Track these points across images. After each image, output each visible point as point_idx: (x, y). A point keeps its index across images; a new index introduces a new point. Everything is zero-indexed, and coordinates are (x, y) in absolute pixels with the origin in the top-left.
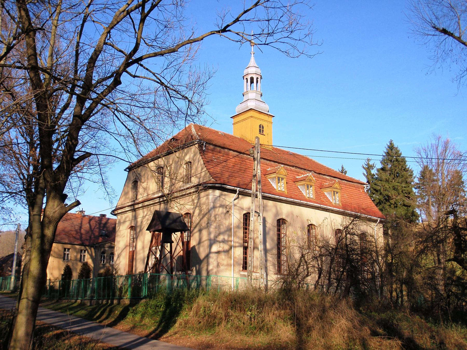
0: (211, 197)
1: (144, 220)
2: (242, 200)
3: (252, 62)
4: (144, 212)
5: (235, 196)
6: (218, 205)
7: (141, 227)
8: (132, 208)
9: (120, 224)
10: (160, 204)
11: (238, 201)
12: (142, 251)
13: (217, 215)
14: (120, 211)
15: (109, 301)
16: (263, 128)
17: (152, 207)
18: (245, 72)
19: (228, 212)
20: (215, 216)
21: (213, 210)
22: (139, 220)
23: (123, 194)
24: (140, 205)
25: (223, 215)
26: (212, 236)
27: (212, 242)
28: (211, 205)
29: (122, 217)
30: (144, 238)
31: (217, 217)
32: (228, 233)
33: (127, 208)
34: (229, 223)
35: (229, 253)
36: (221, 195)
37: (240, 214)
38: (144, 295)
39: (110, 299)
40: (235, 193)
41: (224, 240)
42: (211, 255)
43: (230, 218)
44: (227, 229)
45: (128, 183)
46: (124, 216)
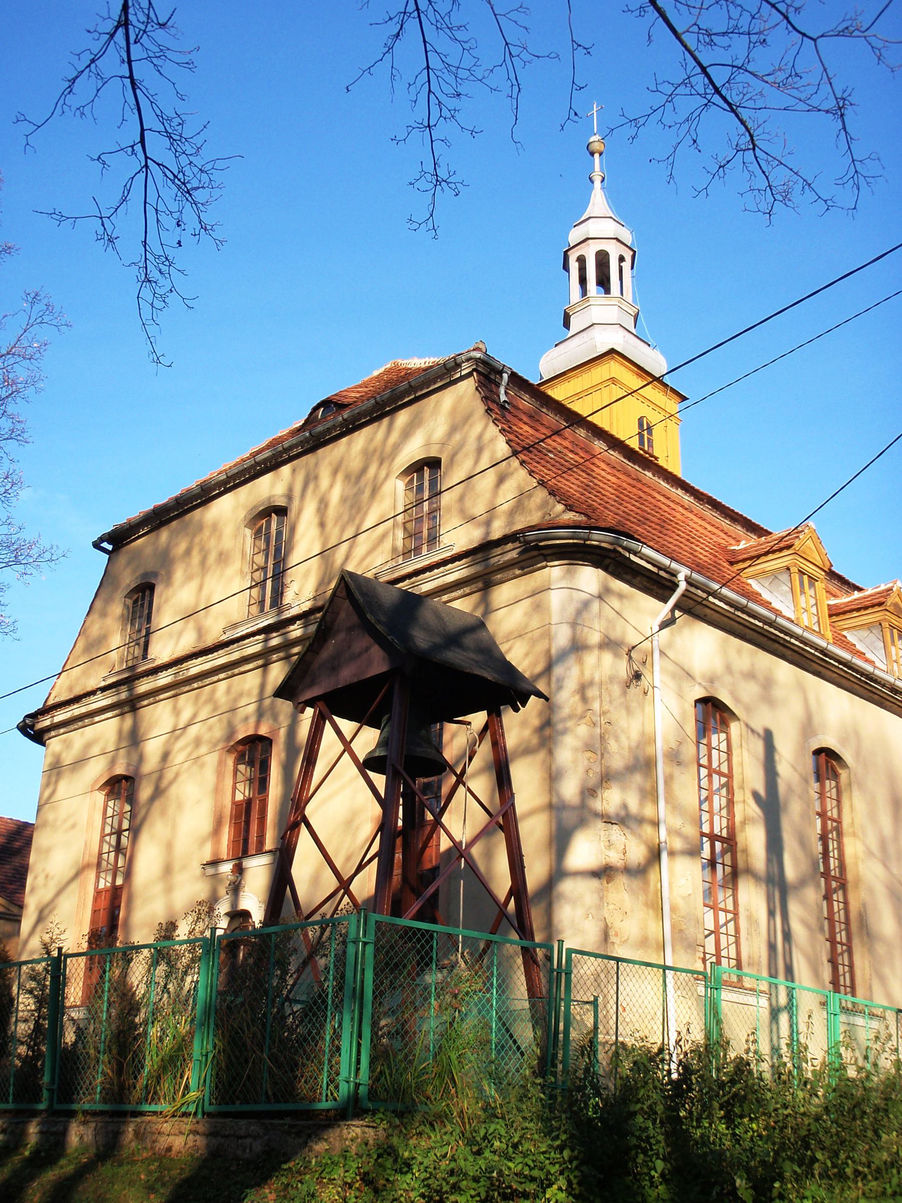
0: (556, 599)
1: (180, 744)
2: (686, 632)
3: (598, 202)
4: (177, 712)
5: (664, 609)
6: (594, 638)
7: (160, 779)
8: (123, 696)
9: (59, 775)
10: (265, 666)
11: (672, 634)
12: (158, 888)
13: (591, 683)
14: (61, 716)
15: (33, 1129)
16: (650, 429)
17: (223, 685)
18: (574, 236)
19: (637, 676)
20: (583, 690)
21: (571, 660)
22: (152, 748)
23: (80, 645)
24: (164, 679)
25: (616, 690)
26: (570, 789)
27: (569, 818)
28: (562, 637)
29: (68, 745)
30: (174, 827)
31: (592, 693)
32: (638, 778)
33: (99, 695)
34: (643, 734)
35: (646, 883)
36: (604, 594)
37: (680, 695)
38: (344, 1089)
39: (34, 1114)
40: (665, 600)
41: (623, 813)
42: (567, 887)
43: (648, 709)
44: (636, 759)
45: (109, 601)
46: (78, 738)
